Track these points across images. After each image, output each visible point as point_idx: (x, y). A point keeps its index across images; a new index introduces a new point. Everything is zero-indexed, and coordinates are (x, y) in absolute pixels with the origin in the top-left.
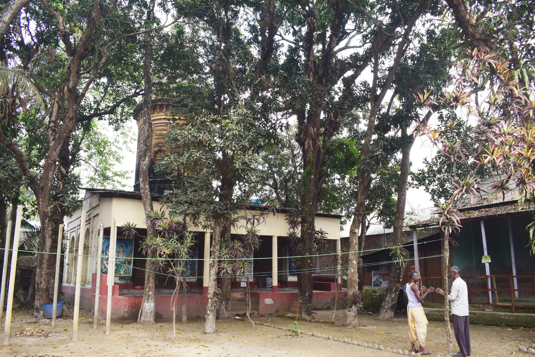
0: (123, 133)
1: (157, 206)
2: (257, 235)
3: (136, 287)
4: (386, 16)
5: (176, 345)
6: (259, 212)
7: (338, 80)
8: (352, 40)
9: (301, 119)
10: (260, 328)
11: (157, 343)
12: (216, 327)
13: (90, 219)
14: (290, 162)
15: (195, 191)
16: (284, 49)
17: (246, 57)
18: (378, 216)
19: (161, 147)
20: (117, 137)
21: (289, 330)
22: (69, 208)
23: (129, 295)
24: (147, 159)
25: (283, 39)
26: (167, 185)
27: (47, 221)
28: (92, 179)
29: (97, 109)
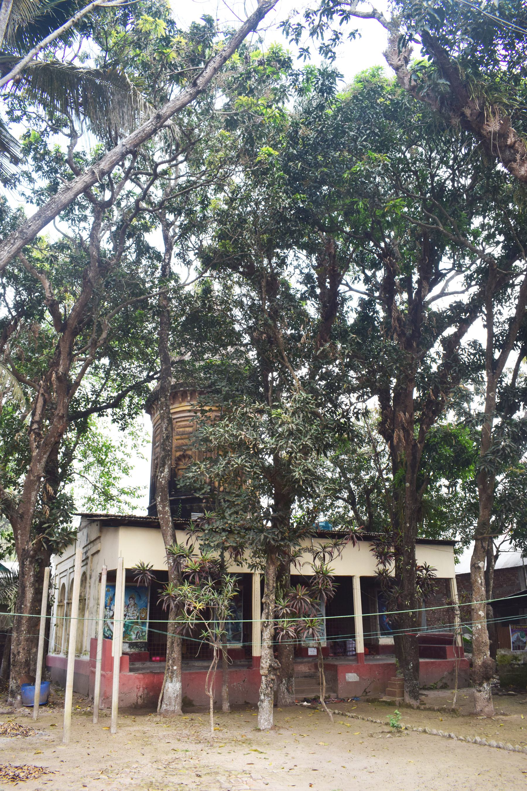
0: (132, 434)
1: (182, 538)
3: (154, 659)
6: (329, 542)
7: (435, 341)
8: (450, 284)
9: (384, 400)
10: (341, 720)
11: (186, 747)
13: (87, 558)
14: (372, 464)
15: (237, 513)
18: (511, 539)
19: (185, 450)
20: (124, 439)
21: (387, 724)
23: (144, 671)
24: (166, 470)
25: (351, 289)
27: (27, 563)
28: (90, 500)
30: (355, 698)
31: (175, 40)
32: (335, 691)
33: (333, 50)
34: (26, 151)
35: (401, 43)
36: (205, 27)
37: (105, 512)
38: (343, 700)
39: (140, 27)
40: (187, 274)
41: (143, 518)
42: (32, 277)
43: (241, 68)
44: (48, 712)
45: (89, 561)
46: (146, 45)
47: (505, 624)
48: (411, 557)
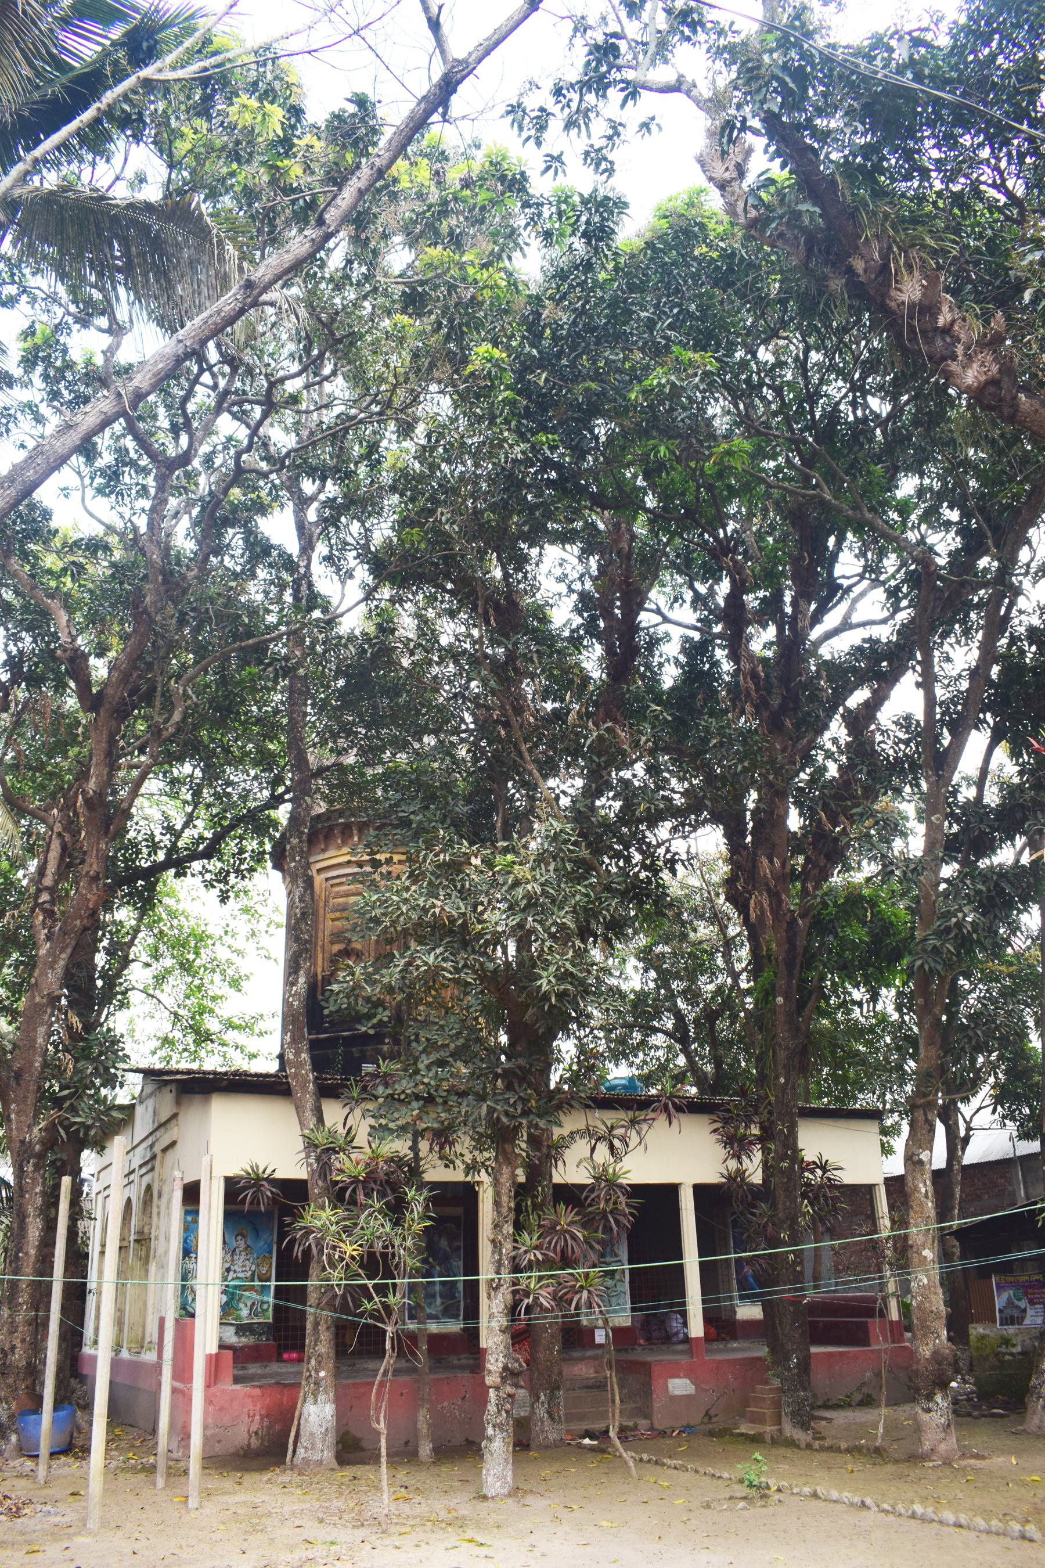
0: (246, 910)
1: (334, 1113)
2: (620, 1186)
3: (285, 1356)
4: (947, 531)
5: (387, 1541)
6: (620, 1116)
7: (830, 718)
8: (858, 605)
9: (734, 835)
10: (651, 1474)
11: (335, 1534)
12: (514, 1475)
13: (154, 1157)
14: (720, 962)
15: (441, 1063)
16: (672, 649)
17: (567, 680)
18: (996, 1104)
20: (230, 921)
21: (741, 1481)
22: (88, 1128)
23: (264, 1382)
24: (302, 980)
25: (666, 620)
26: (369, 1049)
27: (29, 1168)
28: (166, 1041)
29: (173, 848)
30: (687, 1428)
31: (302, 143)
32: (647, 1416)
33: (610, 157)
34: (29, 362)
35: (727, 134)
36: (353, 115)
37: (195, 1066)
38: (663, 1434)
39: (233, 118)
40: (349, 600)
41: (267, 1075)
42: (36, 605)
43: (434, 195)
44: (67, 1466)
45: (157, 1163)
46: (250, 154)
47: (984, 1273)
48: (790, 1142)
